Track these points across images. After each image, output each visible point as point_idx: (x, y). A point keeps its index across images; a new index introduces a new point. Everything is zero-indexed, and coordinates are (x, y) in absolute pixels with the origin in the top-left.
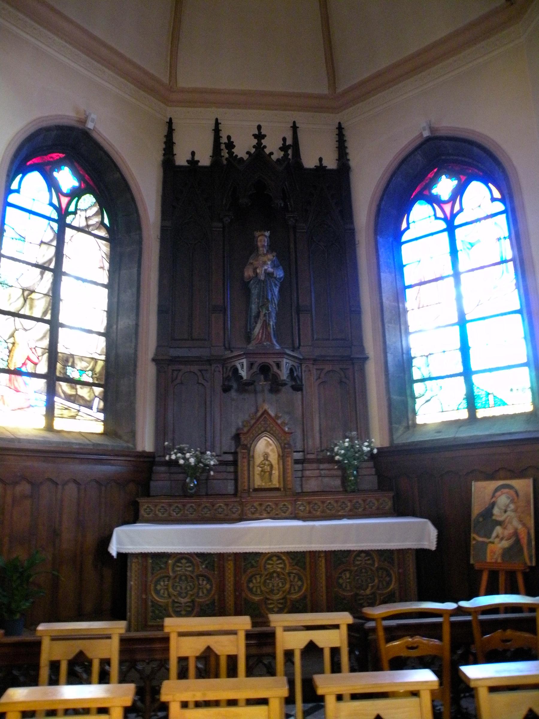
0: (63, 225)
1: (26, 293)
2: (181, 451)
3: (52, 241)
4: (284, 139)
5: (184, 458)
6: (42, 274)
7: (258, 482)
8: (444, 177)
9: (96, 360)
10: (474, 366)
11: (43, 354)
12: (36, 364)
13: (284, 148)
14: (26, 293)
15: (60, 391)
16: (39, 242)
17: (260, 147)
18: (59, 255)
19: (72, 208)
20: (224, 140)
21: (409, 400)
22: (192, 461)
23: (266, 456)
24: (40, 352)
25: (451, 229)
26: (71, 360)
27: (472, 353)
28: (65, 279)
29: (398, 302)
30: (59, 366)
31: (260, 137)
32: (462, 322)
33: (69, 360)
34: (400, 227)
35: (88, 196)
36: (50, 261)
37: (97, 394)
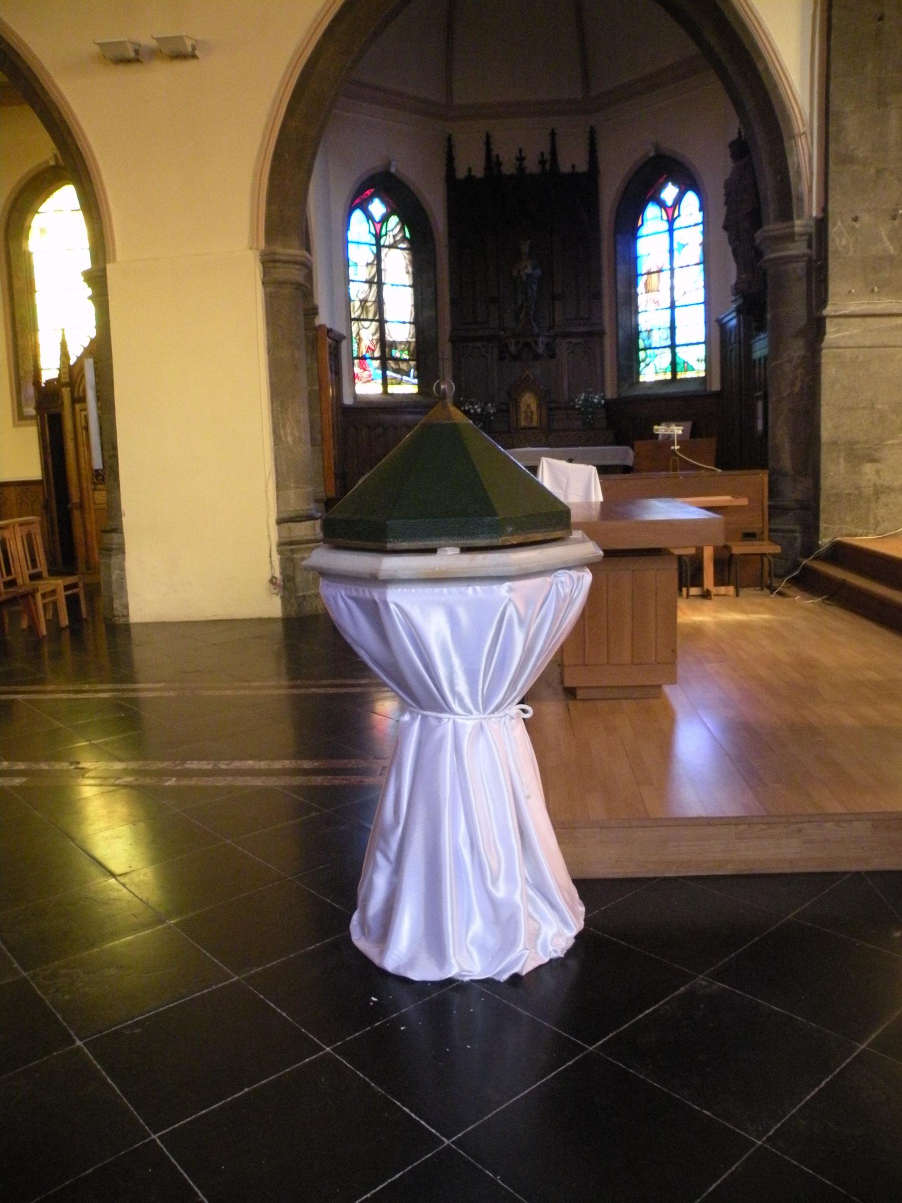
0: (379, 246)
1: (363, 303)
2: (472, 403)
3: (373, 261)
4: (542, 154)
5: (473, 408)
6: (370, 287)
7: (523, 423)
8: (670, 184)
9: (409, 343)
10: (678, 342)
11: (377, 344)
12: (373, 351)
13: (542, 162)
14: (363, 303)
15: (390, 367)
16: (365, 264)
17: (521, 169)
18: (379, 271)
19: (383, 232)
20: (494, 159)
21: (635, 364)
22: (479, 410)
23: (529, 406)
24: (375, 342)
25: (671, 231)
26: (394, 345)
27: (677, 331)
28: (385, 287)
29: (631, 288)
30: (387, 350)
31: (521, 159)
32: (673, 307)
33: (394, 345)
34: (637, 224)
35: (393, 217)
36: (374, 277)
37: (412, 366)
